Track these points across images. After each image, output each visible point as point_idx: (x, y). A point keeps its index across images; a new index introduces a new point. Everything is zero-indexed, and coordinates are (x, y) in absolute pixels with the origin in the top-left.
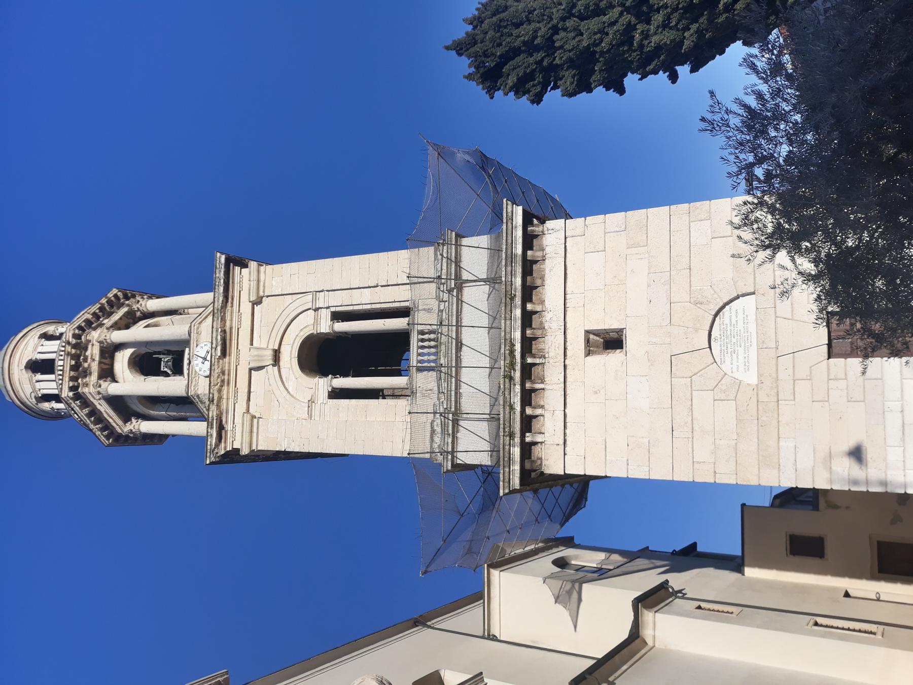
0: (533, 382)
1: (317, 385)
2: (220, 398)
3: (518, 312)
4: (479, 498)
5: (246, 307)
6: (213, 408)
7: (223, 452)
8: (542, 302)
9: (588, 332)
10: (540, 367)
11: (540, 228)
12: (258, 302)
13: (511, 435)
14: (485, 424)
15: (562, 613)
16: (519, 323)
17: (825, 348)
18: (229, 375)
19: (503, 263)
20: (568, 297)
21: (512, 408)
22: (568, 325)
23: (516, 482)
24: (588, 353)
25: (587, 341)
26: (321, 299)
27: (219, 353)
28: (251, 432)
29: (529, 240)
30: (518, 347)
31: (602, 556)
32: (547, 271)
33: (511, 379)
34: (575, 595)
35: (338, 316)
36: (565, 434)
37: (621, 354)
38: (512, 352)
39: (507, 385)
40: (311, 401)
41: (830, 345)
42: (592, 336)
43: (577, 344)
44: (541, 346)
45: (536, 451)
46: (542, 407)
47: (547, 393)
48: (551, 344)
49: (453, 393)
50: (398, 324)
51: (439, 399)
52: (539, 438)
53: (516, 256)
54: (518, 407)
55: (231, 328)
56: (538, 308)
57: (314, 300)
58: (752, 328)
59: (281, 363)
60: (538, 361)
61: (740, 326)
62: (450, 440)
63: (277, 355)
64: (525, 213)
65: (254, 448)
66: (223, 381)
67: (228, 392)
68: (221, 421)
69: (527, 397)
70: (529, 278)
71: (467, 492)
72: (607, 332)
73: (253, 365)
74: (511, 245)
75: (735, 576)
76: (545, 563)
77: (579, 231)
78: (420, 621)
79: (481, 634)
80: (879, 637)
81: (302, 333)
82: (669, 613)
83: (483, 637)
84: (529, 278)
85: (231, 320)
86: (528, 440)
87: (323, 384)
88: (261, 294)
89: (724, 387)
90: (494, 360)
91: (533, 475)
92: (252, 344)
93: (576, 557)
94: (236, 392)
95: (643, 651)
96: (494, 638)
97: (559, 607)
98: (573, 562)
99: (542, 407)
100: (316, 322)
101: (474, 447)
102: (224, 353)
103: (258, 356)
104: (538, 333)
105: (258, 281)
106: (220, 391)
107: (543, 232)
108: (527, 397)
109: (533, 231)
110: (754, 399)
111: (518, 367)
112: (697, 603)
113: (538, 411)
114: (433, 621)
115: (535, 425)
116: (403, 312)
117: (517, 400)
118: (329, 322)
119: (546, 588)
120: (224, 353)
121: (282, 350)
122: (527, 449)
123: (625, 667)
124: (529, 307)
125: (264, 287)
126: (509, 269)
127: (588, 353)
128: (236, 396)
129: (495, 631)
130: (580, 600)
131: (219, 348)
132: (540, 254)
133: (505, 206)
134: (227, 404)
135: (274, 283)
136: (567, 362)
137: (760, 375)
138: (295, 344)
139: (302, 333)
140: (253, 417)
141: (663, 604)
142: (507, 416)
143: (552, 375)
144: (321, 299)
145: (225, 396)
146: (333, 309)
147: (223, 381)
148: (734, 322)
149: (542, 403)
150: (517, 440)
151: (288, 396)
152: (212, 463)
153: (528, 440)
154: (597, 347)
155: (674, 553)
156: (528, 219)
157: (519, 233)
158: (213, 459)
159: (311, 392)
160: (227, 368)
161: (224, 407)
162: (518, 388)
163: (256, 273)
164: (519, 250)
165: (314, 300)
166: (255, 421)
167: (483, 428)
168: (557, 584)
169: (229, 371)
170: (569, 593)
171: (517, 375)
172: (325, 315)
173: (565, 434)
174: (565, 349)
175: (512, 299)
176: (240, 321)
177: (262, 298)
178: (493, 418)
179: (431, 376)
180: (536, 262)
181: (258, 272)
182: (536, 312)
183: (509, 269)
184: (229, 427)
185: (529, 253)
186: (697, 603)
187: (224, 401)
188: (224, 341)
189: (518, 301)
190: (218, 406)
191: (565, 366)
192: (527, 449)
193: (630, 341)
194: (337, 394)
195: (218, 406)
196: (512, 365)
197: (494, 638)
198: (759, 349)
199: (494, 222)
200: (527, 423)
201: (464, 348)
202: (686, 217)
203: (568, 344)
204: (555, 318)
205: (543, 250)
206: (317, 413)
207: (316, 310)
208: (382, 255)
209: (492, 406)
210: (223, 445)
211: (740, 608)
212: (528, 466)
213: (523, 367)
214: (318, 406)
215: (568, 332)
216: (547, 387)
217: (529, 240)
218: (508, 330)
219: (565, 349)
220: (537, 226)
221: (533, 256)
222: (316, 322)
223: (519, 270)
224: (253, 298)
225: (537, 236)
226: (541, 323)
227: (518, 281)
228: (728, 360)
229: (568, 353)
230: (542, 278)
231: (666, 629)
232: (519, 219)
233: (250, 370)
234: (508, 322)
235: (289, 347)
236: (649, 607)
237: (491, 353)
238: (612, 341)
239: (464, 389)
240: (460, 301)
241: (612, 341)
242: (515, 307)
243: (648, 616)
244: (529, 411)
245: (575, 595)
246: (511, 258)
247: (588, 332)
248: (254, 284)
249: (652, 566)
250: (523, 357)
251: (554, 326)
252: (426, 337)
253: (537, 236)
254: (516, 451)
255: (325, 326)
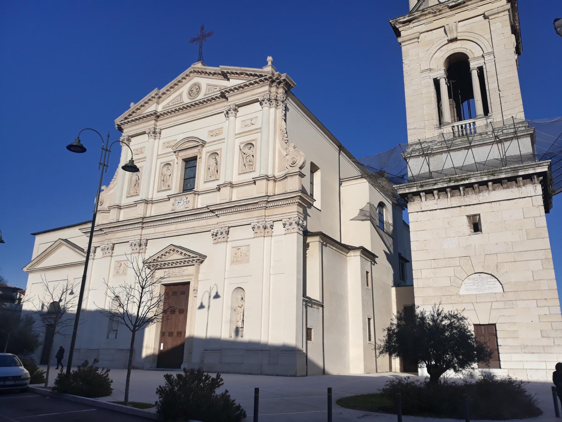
0: (450, 192)
1: (440, 70)
2: (426, 15)
3: (485, 179)
4: (391, 176)
5: (481, 10)
6: (419, 13)
7: (397, 27)
8: (494, 190)
9: (479, 215)
10: (459, 194)
11: (536, 182)
12: (486, 17)
13: (422, 186)
14: (428, 170)
15: (356, 213)
16: (480, 180)
17: (478, 323)
18: (440, 14)
19: (512, 166)
20: (498, 203)
21: (435, 184)
22: (482, 205)
23: (401, 192)
24: (468, 217)
25: (475, 215)
26: (490, 58)
27: (450, 5)
28: (410, 40)
29: (529, 178)
30: (467, 182)
31: (391, 221)
32: (511, 190)
33: (450, 181)
34: (365, 218)
35: (481, 70)
36: (427, 211)
37: (469, 232)
38: (464, 179)
39: (446, 180)
40: (430, 70)
41: (480, 325)
42: (478, 217)
43: (472, 211)
44: (470, 193)
45: (417, 198)
46: (439, 198)
47: (446, 199)
48: (472, 198)
49: (441, 150)
50: (479, 109)
51: (438, 142)
52: (423, 199)
53: (518, 172)
54: (436, 187)
55: (467, 5)
56: (490, 188)
57: (489, 54)
58: (487, 291)
59: (450, 44)
60: (462, 192)
61: (487, 286)
62: (417, 154)
63: (455, 40)
64: (546, 172)
65: (403, 44)
66: (435, 12)
67: (430, 18)
68: (413, 20)
69: (442, 190)
70: (506, 181)
71: (393, 171)
72: (480, 224)
73: (447, 27)
74: (523, 168)
75: (392, 284)
76: (380, 197)
77: (535, 204)
78: (341, 148)
79: (341, 177)
80: (368, 342)
81: (468, 51)
82: (361, 261)
83: (340, 179)
84: (506, 181)
85: (472, 4)
86: (421, 194)
87: (441, 73)
88: (490, 18)
89: (456, 281)
90: (461, 168)
91: (406, 198)
92: (459, 22)
93: (387, 210)
94: (431, 22)
95: (344, 253)
96: (340, 185)
97: (358, 211)
98: (384, 210)
99: (439, 198)
100: (475, 59)
101: (416, 167)
102: (451, 8)
103: (452, 30)
104: (477, 190)
105: (498, 13)
106: (429, 13)
107: (535, 183)
108: (442, 190)
109: (534, 178)
110: (452, 294)
111: (456, 184)
112: (369, 271)
113: (436, 197)
114: (343, 153)
115: (429, 196)
116: (486, 111)
117: (439, 186)
118: (476, 66)
119: (365, 204)
120: (451, 8)
121: (458, 42)
122: (417, 194)
123: (334, 248)
124: (490, 184)
125: (495, 18)
126: (509, 170)
127: (468, 217)
128: (428, 23)
129: (344, 184)
130: (363, 220)
131: (454, 4)
132: (521, 184)
133: (547, 161)
134: (423, 20)
135: (497, 24)
136: (463, 207)
137: (463, 296)
138: (462, 49)
139: (468, 51)
140: (418, 38)
141: (366, 258)
142: (430, 183)
143: (455, 201)
144: (490, 58)
145: (427, 17)
146: (484, 67)
147: (435, 12)
148: (489, 283)
149: (441, 197)
150: (420, 189)
151: (432, 55)
152: (390, 23)
153: (421, 194)
154: (473, 220)
155: (400, 254)
156: (539, 174)
157: (531, 171)
158: (392, 23)
159: (436, 68)
160: (443, 12)
161: (421, 18)
162: (446, 185)
163: (503, 10)
164: (521, 173)
165: (489, 54)
166: (416, 40)
167: (425, 169)
168: (368, 209)
169: (442, 14)
170: (365, 215)
171: (452, 184)
172: (480, 63)
173: (427, 211)
174: (469, 205)
175: (493, 175)
176: (472, 9)
177: (488, 18)
178: (430, 175)
179: (450, 135)
180: (516, 182)
181: (504, 11)
182: (488, 187)
183: (509, 170)
184: (411, 25)
185: (521, 178)
186: (369, 271)
187: (425, 17)
188: (459, 4)
189: (492, 178)
190: (421, 16)
191: (460, 206)
192: (417, 194)
193: (477, 237)
194: (436, 82)
195: (421, 16)
196: (457, 181)
197: (340, 185)
198: (476, 295)
199: (537, 156)
200: (429, 192)
201: (466, 151)
202: (544, 257)
203: (472, 206)
204: (485, 197)
205: (524, 185)
206: (425, 75)
207: (483, 56)
208: (518, 90)
209: (437, 172)
210: (401, 25)
211: (371, 289)
212: (409, 196)
213: (456, 185)
214: (428, 74)
215: (479, 205)
216: (449, 199)
217: (529, 178)
218: (475, 175)
219: (469, 205)
220: (538, 179)
221: (519, 181)
222: (475, 59)
223: (509, 175)
224: (486, 14)
225: (532, 180)
226: (483, 191)
227: (503, 176)
228: (470, 281)
229: (468, 207)
230: (508, 187)
231: (354, 261)
232: (539, 170)
233: (444, 26)
234: (479, 175)
235: (459, 46)
236: (362, 252)
237: (466, 166)
238: (476, 227)
239: (444, 155)
240: (492, 143)
241: (476, 227)
242: (488, 177)
243: (358, 253)
244: (435, 192)
245: (365, 218)
246: (516, 170)
247: (479, 215)
248: (496, 11)
249: (389, 246)
250: (462, 185)
251: (481, 198)
252: (472, 127)
253: (532, 180)
254: (414, 190)
255: (474, 65)
